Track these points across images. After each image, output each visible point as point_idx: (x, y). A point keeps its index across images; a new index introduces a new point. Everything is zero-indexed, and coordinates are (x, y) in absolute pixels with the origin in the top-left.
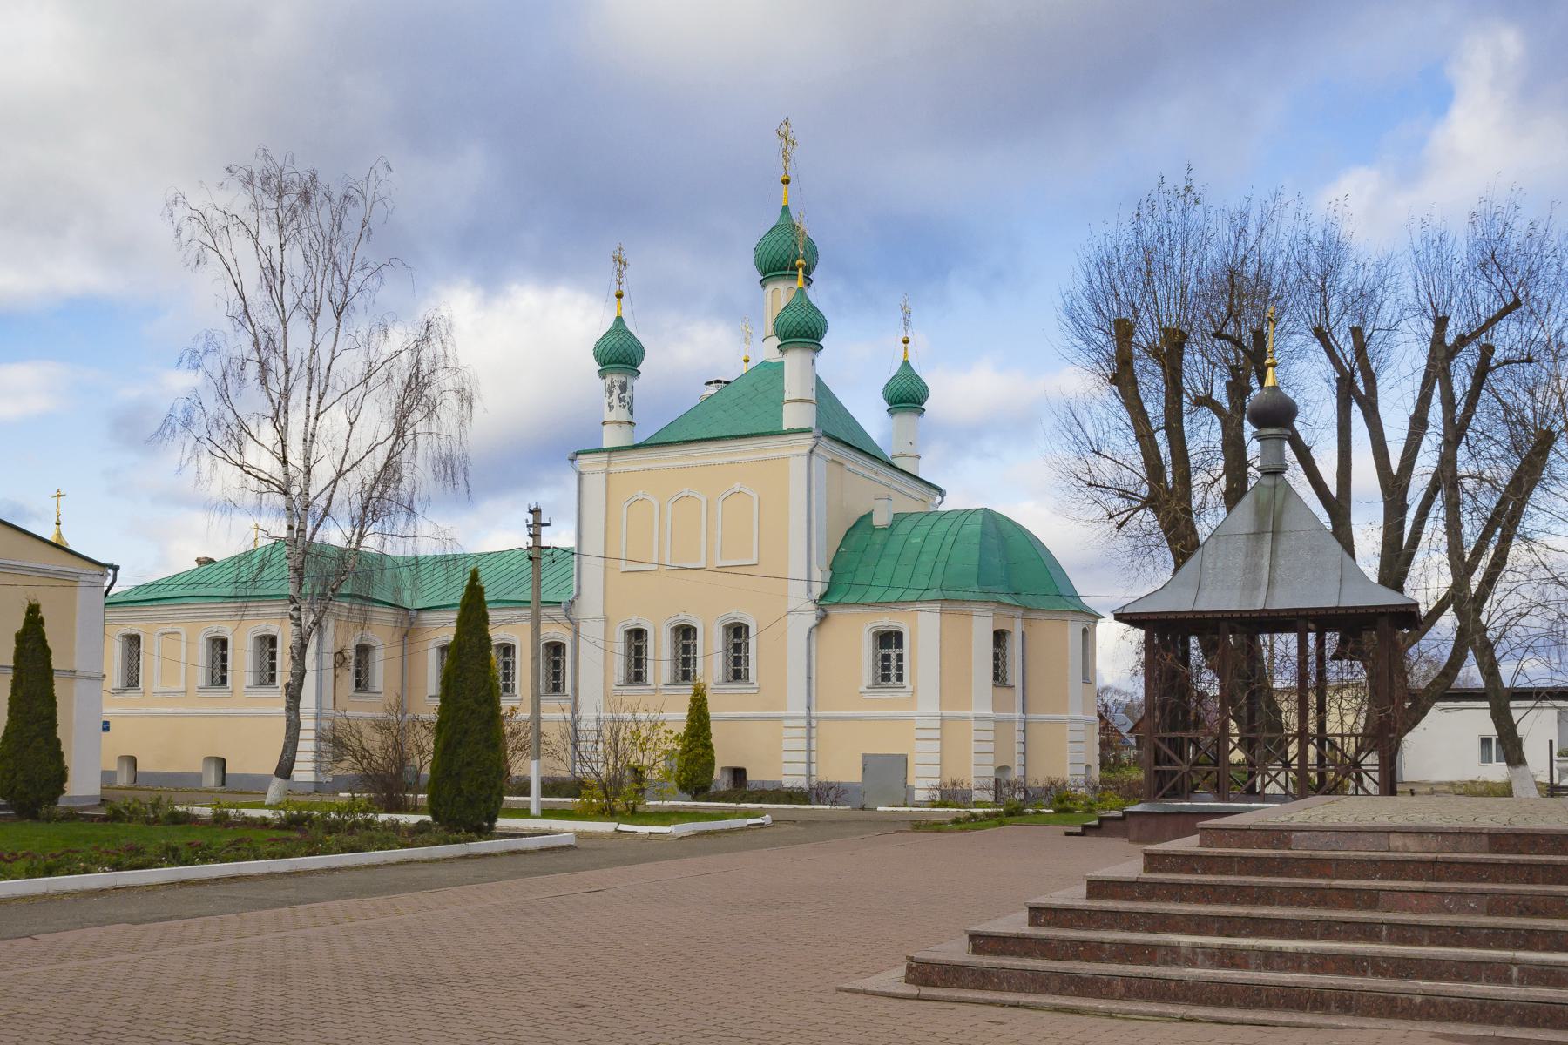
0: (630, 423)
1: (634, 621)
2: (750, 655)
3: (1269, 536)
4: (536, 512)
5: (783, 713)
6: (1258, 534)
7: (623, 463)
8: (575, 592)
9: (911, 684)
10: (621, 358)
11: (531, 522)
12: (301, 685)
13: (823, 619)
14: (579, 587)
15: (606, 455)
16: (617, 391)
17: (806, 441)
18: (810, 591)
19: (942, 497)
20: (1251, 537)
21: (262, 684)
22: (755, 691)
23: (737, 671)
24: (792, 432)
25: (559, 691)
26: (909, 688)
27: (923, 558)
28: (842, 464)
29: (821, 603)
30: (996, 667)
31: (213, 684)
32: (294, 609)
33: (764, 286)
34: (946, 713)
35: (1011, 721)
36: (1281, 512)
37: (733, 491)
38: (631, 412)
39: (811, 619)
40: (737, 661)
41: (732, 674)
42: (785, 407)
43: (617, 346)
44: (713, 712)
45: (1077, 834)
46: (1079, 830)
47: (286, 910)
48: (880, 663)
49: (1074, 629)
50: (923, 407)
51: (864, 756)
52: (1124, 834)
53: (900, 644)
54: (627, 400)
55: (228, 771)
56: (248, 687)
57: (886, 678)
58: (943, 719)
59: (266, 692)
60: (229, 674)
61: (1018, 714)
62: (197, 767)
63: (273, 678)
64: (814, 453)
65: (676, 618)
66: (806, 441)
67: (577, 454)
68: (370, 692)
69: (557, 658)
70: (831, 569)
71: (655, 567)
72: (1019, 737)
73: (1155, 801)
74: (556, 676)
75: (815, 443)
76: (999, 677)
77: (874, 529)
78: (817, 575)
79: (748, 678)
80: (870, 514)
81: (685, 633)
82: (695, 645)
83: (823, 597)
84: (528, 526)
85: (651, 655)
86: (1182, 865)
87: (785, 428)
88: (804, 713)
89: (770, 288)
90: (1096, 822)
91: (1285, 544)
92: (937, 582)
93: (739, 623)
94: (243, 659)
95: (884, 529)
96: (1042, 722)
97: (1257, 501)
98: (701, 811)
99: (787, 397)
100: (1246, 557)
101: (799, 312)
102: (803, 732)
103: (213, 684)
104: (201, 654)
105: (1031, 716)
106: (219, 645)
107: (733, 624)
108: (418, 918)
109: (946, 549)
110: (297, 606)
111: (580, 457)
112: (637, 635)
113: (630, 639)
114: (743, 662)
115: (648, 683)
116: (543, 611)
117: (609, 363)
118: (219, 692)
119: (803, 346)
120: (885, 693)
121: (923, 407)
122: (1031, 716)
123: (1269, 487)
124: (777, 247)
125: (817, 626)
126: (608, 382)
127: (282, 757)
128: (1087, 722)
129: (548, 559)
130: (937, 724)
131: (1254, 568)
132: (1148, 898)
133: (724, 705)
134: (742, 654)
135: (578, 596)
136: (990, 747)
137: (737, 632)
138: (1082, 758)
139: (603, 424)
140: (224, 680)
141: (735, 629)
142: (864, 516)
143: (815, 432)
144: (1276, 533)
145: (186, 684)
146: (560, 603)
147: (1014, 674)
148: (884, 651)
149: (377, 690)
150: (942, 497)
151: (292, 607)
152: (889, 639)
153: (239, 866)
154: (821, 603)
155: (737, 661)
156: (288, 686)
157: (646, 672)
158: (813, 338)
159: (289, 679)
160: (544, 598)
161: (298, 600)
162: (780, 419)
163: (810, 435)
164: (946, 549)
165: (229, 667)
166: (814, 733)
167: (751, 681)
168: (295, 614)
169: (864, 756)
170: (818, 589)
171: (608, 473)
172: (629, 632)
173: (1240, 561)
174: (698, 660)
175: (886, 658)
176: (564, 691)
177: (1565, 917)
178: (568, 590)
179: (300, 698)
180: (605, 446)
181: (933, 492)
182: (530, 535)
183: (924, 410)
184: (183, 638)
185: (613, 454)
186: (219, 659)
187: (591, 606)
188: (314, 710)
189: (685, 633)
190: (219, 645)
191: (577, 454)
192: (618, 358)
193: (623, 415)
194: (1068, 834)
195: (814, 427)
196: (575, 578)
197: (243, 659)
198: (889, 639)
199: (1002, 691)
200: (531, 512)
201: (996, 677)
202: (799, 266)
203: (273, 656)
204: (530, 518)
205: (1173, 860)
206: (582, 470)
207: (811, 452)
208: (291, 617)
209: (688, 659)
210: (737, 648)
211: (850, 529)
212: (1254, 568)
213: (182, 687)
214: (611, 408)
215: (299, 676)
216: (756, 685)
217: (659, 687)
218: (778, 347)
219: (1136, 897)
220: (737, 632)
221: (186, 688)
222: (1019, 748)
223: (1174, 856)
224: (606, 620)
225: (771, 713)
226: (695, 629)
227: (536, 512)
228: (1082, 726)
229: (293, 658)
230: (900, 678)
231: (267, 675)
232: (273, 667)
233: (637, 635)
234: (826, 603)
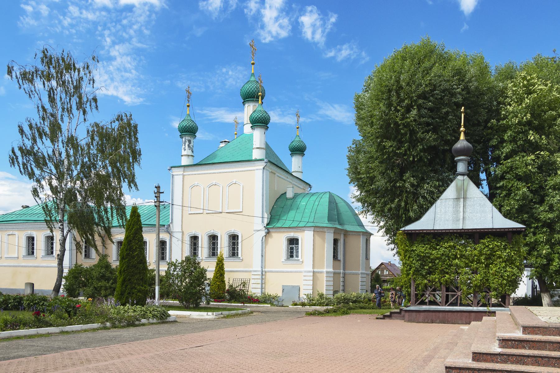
0: (192, 156)
1: (193, 232)
2: (239, 246)
3: (462, 200)
4: (158, 187)
5: (251, 269)
6: (458, 199)
7: (190, 172)
8: (170, 221)
9: (201, 256)
10: (189, 130)
11: (156, 192)
12: (63, 255)
13: (268, 233)
14: (172, 219)
15: (183, 168)
16: (187, 143)
17: (261, 165)
18: (263, 222)
19: (311, 188)
20: (455, 200)
21: (48, 255)
22: (241, 261)
23: (234, 253)
24: (256, 160)
25: (164, 260)
26: (301, 260)
27: (306, 210)
28: (275, 174)
29: (267, 227)
30: (334, 253)
31: (29, 254)
32: (61, 225)
33: (244, 105)
34: (315, 270)
35: (340, 273)
36: (466, 191)
37: (233, 183)
38: (193, 152)
39: (263, 233)
40: (234, 249)
41: (232, 253)
42: (254, 151)
43: (188, 125)
44: (226, 268)
45: (381, 319)
46: (382, 317)
47: (58, 355)
48: (289, 251)
49: (362, 240)
50: (304, 153)
51: (283, 285)
52: (403, 318)
53: (297, 244)
54: (191, 147)
55: (35, 288)
56: (43, 256)
57: (292, 256)
58: (314, 272)
59: (50, 258)
60: (35, 251)
61: (342, 271)
62: (23, 287)
63: (52, 253)
64: (265, 169)
65: (210, 232)
66: (261, 165)
67: (172, 167)
68: (90, 258)
69: (163, 247)
70: (271, 214)
71: (201, 211)
72: (342, 279)
73: (415, 306)
74: (163, 254)
75: (265, 165)
76: (335, 257)
77: (287, 199)
78: (266, 215)
79: (238, 256)
80: (285, 193)
81: (213, 238)
82: (217, 243)
83: (268, 224)
84: (155, 193)
85: (200, 245)
86: (518, 345)
87: (253, 158)
88: (260, 269)
89: (246, 105)
90: (389, 314)
91: (468, 202)
92: (312, 220)
93: (235, 234)
94: (40, 245)
95: (292, 199)
96: (350, 274)
97: (457, 185)
98: (220, 307)
99: (254, 146)
100: (454, 208)
101: (259, 113)
102: (260, 277)
103: (29, 254)
104: (23, 243)
105: (347, 272)
106: (31, 240)
107: (232, 235)
108: (122, 362)
109: (315, 207)
110: (62, 223)
111: (172, 169)
112: (194, 239)
113: (191, 240)
114: (236, 249)
115: (199, 257)
116: (160, 229)
117: (184, 132)
118: (30, 258)
119: (261, 127)
120: (290, 262)
121: (304, 153)
122: (347, 272)
123: (461, 180)
124: (249, 89)
125: (265, 236)
126: (184, 139)
127: (56, 283)
128: (366, 274)
129: (163, 207)
130: (312, 274)
131: (457, 212)
132: (505, 362)
133: (228, 266)
134: (236, 246)
135: (172, 222)
136: (332, 283)
137: (234, 238)
138: (365, 287)
139: (182, 156)
140: (33, 253)
141: (233, 237)
142: (283, 194)
143: (266, 160)
144: (465, 198)
145: (18, 254)
146: (165, 225)
147: (340, 256)
148: (291, 246)
149: (93, 258)
150: (311, 188)
151: (60, 224)
152: (293, 242)
153: (37, 330)
154: (267, 227)
155: (234, 249)
156: (58, 255)
157: (198, 252)
158: (265, 124)
159: (59, 253)
160: (160, 224)
161: (62, 221)
162: (251, 155)
163: (263, 162)
164: (315, 207)
165: (35, 248)
166: (264, 277)
167: (239, 257)
168: (61, 227)
169: (283, 285)
170: (266, 221)
171: (184, 176)
172: (191, 237)
173: (451, 209)
174: (218, 249)
175: (292, 248)
176: (166, 259)
177: (559, 351)
178: (167, 220)
179: (63, 260)
180: (183, 164)
181: (308, 186)
182: (156, 197)
183: (304, 154)
184: (17, 236)
185: (186, 168)
186: (31, 245)
187: (176, 227)
188: (68, 265)
189: (213, 238)
190: (31, 240)
191: (172, 167)
192: (189, 129)
193: (190, 153)
194: (377, 318)
195: (265, 158)
196: (170, 215)
197: (40, 245)
198: (293, 242)
199: (337, 262)
200: (156, 187)
201: (334, 256)
202: (260, 95)
203: (52, 244)
204: (156, 190)
205: (513, 342)
206: (173, 174)
207: (264, 168)
208: (60, 228)
209: (215, 248)
210: (234, 244)
211: (277, 199)
212: (457, 212)
213: (16, 255)
214: (185, 150)
215: (63, 251)
216: (241, 258)
217: (203, 258)
218: (251, 127)
219: (498, 362)
220: (234, 238)
221: (18, 256)
222: (341, 284)
223: (514, 340)
224: (183, 232)
225: (247, 269)
226: (217, 236)
227: (158, 187)
228: (365, 276)
229: (60, 244)
230: (297, 256)
231: (50, 251)
232: (52, 248)
233: (194, 239)
234: (270, 227)
